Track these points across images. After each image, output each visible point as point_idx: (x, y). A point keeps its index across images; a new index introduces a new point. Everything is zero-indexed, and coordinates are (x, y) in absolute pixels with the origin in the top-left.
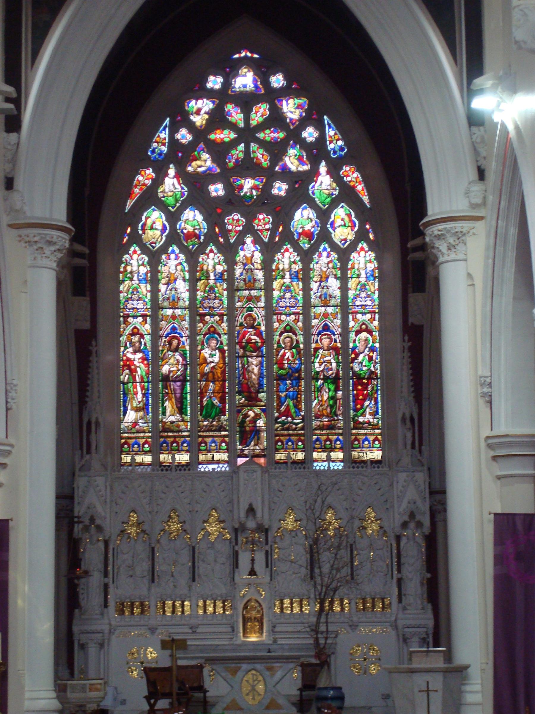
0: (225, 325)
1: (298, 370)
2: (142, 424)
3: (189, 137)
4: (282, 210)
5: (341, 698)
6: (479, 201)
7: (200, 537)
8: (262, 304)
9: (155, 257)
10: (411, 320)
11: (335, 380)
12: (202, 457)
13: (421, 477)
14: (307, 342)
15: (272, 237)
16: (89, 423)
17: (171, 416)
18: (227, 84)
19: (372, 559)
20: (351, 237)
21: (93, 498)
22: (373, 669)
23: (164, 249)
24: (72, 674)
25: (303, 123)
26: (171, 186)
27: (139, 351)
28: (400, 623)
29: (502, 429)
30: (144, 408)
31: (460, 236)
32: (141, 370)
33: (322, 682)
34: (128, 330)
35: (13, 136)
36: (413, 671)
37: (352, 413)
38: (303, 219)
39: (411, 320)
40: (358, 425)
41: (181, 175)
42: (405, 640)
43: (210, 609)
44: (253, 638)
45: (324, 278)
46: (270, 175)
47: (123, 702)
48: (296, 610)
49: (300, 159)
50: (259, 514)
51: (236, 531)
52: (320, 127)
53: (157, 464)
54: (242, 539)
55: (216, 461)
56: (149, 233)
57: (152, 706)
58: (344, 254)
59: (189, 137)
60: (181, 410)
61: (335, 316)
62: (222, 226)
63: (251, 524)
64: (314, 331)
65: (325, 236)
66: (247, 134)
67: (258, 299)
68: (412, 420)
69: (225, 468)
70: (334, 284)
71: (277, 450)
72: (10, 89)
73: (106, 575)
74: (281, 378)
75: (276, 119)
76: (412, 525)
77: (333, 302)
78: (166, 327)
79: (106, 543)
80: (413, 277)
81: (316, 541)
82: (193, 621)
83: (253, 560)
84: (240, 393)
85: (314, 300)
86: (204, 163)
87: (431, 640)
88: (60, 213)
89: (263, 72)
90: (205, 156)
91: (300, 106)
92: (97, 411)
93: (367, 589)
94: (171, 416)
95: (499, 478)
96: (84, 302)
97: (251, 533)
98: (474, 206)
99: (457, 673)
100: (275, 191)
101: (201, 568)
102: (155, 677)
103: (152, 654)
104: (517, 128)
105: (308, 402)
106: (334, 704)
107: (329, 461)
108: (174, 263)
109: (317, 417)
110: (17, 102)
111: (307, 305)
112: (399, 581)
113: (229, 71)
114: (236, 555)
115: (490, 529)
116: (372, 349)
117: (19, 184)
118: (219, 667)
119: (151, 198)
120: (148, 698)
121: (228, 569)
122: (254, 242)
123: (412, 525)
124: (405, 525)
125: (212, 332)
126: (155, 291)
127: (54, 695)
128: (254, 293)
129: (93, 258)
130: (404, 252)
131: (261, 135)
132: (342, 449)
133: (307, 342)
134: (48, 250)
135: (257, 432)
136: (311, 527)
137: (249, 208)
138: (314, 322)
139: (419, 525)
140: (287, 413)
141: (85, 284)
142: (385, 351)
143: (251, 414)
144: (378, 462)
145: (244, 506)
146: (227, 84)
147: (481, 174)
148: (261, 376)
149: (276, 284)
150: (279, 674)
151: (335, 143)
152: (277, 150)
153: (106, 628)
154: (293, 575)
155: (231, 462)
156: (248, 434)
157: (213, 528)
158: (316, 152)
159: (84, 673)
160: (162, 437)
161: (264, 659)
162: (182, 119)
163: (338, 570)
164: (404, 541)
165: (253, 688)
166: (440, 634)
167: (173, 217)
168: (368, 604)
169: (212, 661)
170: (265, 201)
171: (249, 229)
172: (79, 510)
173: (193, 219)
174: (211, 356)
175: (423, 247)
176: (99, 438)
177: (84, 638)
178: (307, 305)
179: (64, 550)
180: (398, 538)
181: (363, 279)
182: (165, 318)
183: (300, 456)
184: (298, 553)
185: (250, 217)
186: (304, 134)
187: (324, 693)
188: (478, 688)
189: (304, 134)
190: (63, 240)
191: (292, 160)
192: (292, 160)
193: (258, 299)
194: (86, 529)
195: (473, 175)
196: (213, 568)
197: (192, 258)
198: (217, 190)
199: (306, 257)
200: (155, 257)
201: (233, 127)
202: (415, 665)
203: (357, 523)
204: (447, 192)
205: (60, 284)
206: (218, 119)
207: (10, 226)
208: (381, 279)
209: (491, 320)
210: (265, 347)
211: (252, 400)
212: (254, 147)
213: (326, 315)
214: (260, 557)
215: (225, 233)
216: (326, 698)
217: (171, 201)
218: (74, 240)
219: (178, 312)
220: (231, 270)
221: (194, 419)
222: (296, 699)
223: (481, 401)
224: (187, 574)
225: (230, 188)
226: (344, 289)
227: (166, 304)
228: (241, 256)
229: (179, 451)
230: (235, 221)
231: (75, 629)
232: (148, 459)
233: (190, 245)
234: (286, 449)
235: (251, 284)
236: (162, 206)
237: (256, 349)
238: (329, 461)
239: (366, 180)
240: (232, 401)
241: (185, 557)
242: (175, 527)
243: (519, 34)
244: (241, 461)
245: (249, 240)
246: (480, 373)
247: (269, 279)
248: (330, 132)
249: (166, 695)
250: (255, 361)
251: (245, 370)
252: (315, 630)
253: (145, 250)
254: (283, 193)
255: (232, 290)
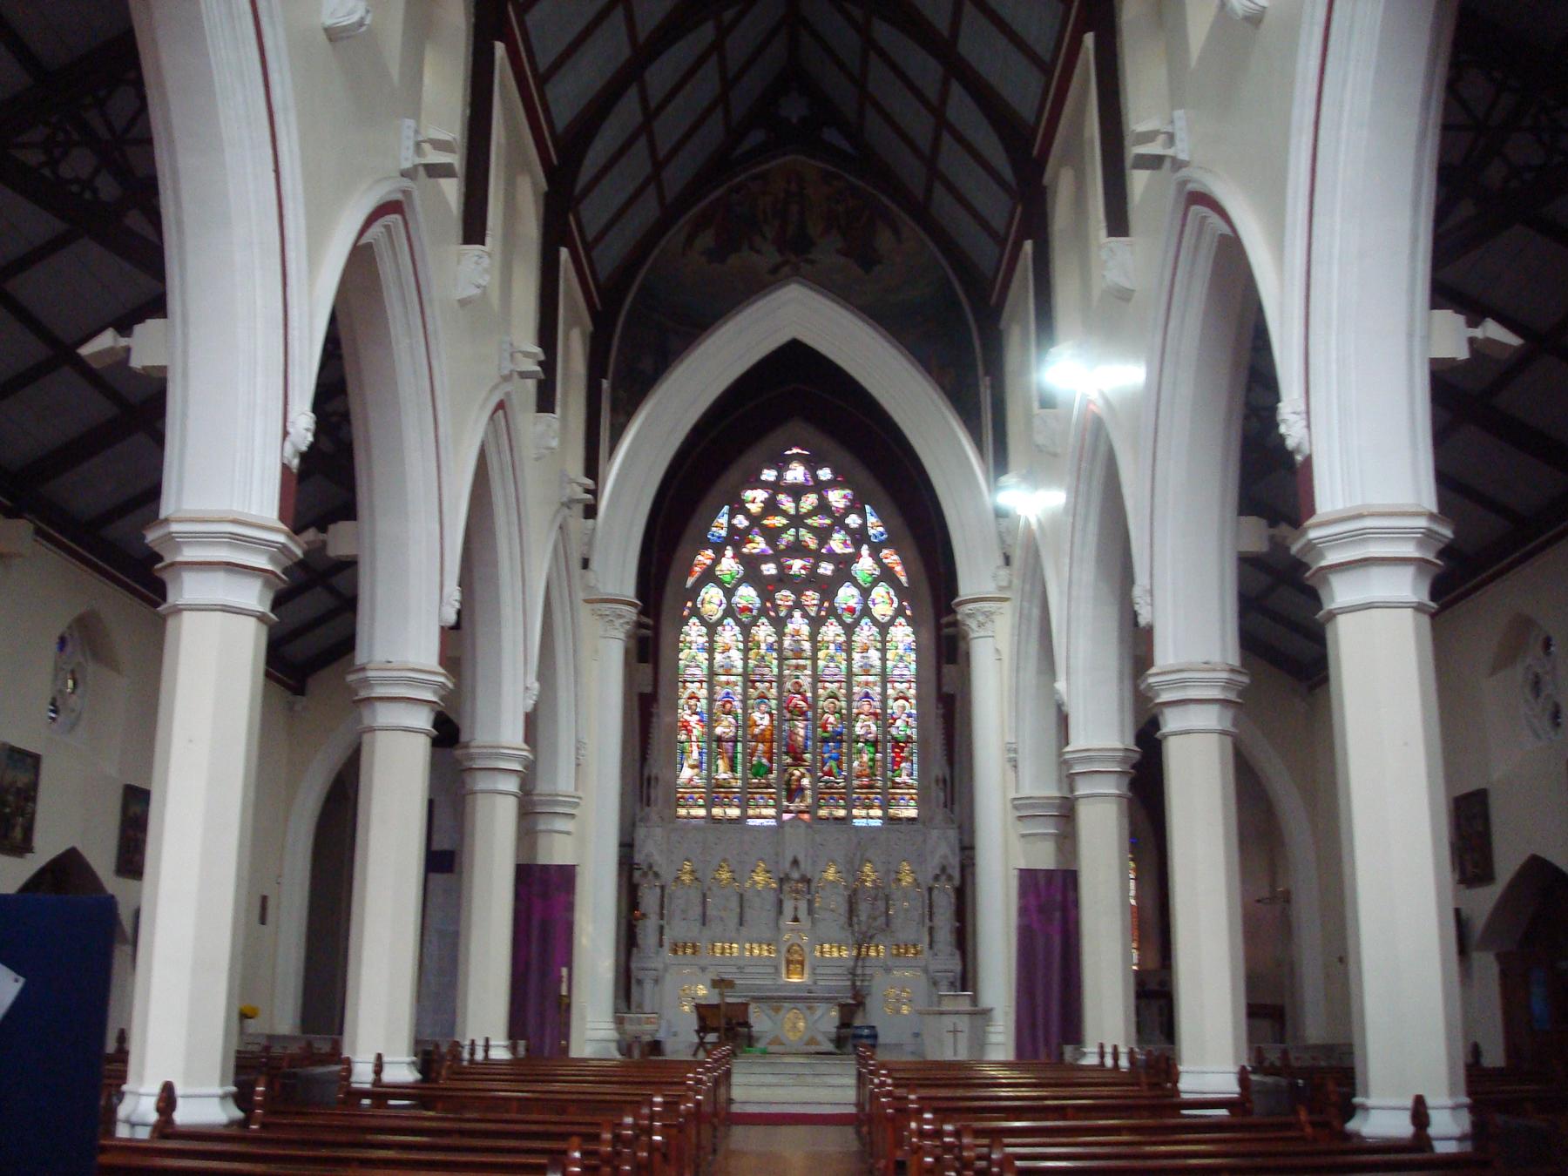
0: (774, 691)
1: (840, 734)
2: (697, 781)
3: (746, 523)
4: (828, 589)
5: (875, 1036)
6: (1004, 584)
7: (747, 885)
8: (808, 672)
9: (712, 628)
10: (945, 689)
11: (875, 743)
12: (751, 812)
13: (952, 834)
14: (849, 708)
15: (819, 612)
16: (649, 780)
17: (723, 774)
18: (780, 477)
19: (905, 908)
20: (890, 612)
21: (651, 846)
22: (905, 1010)
23: (720, 622)
24: (629, 1007)
25: (847, 511)
26: (729, 565)
27: (696, 713)
28: (931, 968)
29: (1027, 791)
30: (698, 766)
31: (988, 615)
32: (697, 731)
33: (857, 1022)
34: (686, 695)
35: (590, 522)
36: (942, 1013)
37: (890, 774)
38: (847, 596)
39: (945, 689)
40: (895, 785)
41: (738, 556)
42: (935, 984)
43: (756, 952)
44: (795, 979)
45: (865, 650)
46: (818, 557)
47: (675, 1034)
48: (836, 954)
49: (844, 543)
50: (802, 866)
51: (781, 881)
52: (863, 515)
53: (710, 818)
54: (786, 888)
55: (764, 816)
56: (707, 606)
57: (701, 1039)
58: (884, 628)
59: (746, 523)
60: (733, 768)
61: (875, 684)
62: (773, 600)
63: (796, 875)
64: (856, 697)
65: (866, 612)
66: (797, 520)
67: (804, 667)
68: (945, 781)
69: (772, 822)
70: (874, 656)
71: (820, 807)
72: (589, 482)
73: (662, 916)
74: (825, 741)
75: (823, 508)
76: (943, 878)
77: (873, 671)
78: (720, 692)
79: (663, 888)
80: (947, 650)
81: (855, 891)
82: (741, 963)
83: (796, 909)
84: (787, 753)
85: (856, 669)
86: (758, 545)
87: (958, 984)
88: (629, 590)
89: (812, 464)
90: (759, 539)
91: (845, 497)
92: (656, 768)
93: (902, 936)
94: (723, 774)
95: (1023, 836)
96: (647, 668)
97: (795, 883)
98: (1001, 589)
99: (982, 1015)
100: (820, 571)
101: (749, 914)
102: (705, 1013)
103: (702, 991)
104: (1039, 521)
105: (850, 762)
106: (869, 1042)
107: (868, 818)
108: (729, 634)
109: (858, 777)
110: (594, 493)
111: (850, 674)
112: (931, 929)
113: (782, 464)
114: (780, 903)
115: (1014, 883)
116: (909, 716)
117: (594, 564)
118: (764, 1006)
119: (709, 576)
120: (698, 1032)
121: (773, 914)
122: (803, 616)
123: (943, 878)
124: (937, 878)
125: (763, 697)
126: (711, 660)
127: (612, 1026)
128: (801, 662)
129: (656, 629)
130: (939, 627)
131: (809, 521)
132: (880, 807)
133: (849, 708)
134: (618, 622)
135: (801, 789)
136: (851, 880)
137: (798, 586)
138: (856, 689)
139: (950, 878)
140: (830, 773)
141: (649, 650)
142: (920, 718)
143: (797, 773)
144: (913, 819)
145: (789, 859)
146: (780, 477)
147: (1007, 560)
148: (806, 738)
149: (821, 654)
150: (819, 1013)
151: (875, 527)
152: (823, 535)
153: (660, 966)
154: (832, 922)
155: (778, 817)
156: (794, 791)
157: (760, 878)
158: (859, 537)
159: (640, 1006)
160: (715, 793)
161: (804, 999)
162: (739, 507)
163: (875, 919)
164: (935, 892)
165: (794, 1027)
166: (966, 979)
167: (729, 593)
168: (900, 950)
169: (757, 999)
170: (812, 580)
171: (798, 605)
172: (639, 858)
173: (747, 595)
174: (762, 720)
175: (955, 624)
176: (657, 793)
177: (641, 975)
178: (850, 674)
179: (624, 891)
180: (930, 890)
181: (901, 652)
182: (720, 684)
183: (841, 813)
184: (838, 902)
185: (799, 593)
186: (847, 521)
187: (859, 1032)
188: (1001, 1029)
189: (847, 521)
190: (631, 614)
191: (838, 543)
192: (838, 543)
193: (804, 667)
194: (645, 874)
195: (1000, 561)
196: (760, 914)
197: (746, 629)
198: (769, 569)
199: (849, 630)
200: (712, 628)
201: (784, 514)
202: (944, 1008)
203: (893, 876)
204: (976, 576)
205: (627, 652)
206: (771, 507)
207: (587, 601)
208: (918, 651)
209: (1017, 691)
210: (811, 713)
211: (798, 760)
212: (803, 531)
213: (867, 684)
214: (803, 905)
215: (776, 607)
216: (861, 1036)
217: (727, 578)
218: (642, 612)
219: (733, 678)
220: (780, 642)
221: (745, 779)
222: (833, 1036)
223: (1008, 766)
224: (736, 920)
225: (781, 567)
226: (884, 659)
227: (721, 671)
228: (790, 628)
229: (730, 806)
230: (784, 597)
231: (633, 965)
232: (702, 812)
233: (744, 618)
234: (828, 806)
235: (798, 653)
236: (719, 583)
237: (803, 713)
238: (868, 818)
239: (905, 562)
240: (780, 760)
241: (734, 904)
242: (725, 875)
243: (1040, 439)
244: (786, 817)
245: (797, 614)
246: (1008, 739)
247: (815, 650)
248: (872, 520)
249: (714, 1030)
250: (801, 724)
251: (792, 733)
252: (853, 973)
253: (703, 622)
254: (829, 573)
255: (782, 659)
